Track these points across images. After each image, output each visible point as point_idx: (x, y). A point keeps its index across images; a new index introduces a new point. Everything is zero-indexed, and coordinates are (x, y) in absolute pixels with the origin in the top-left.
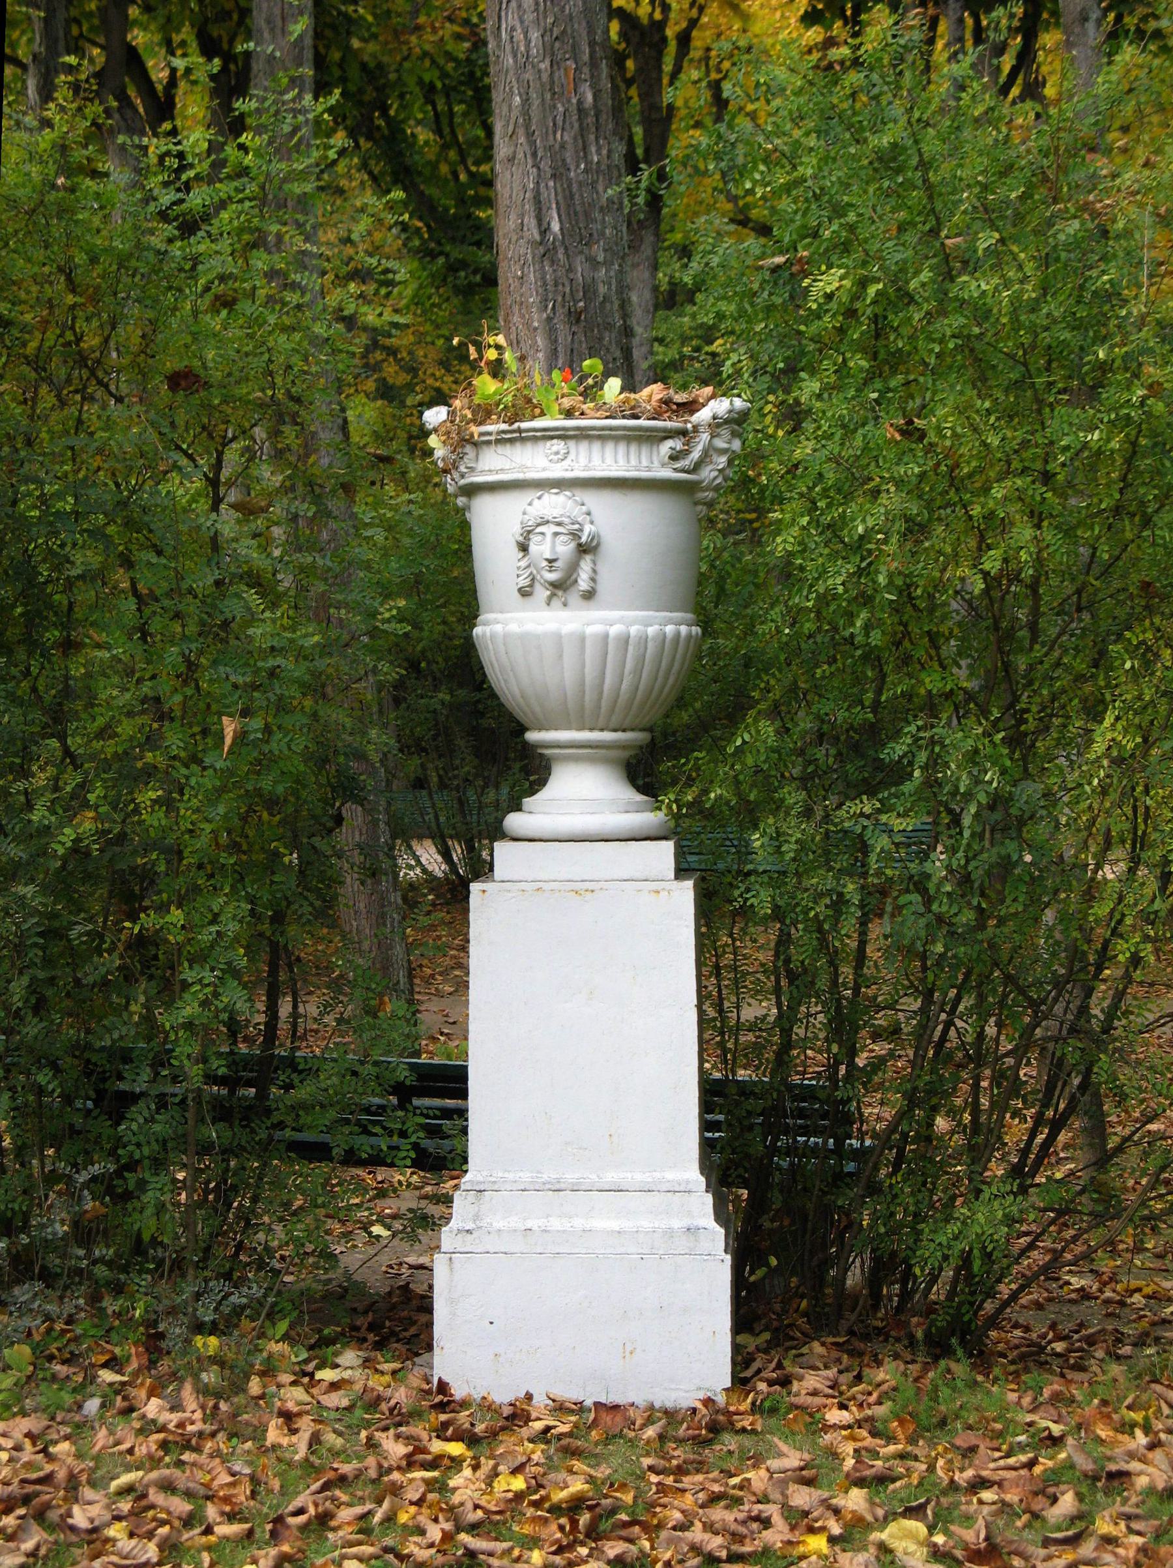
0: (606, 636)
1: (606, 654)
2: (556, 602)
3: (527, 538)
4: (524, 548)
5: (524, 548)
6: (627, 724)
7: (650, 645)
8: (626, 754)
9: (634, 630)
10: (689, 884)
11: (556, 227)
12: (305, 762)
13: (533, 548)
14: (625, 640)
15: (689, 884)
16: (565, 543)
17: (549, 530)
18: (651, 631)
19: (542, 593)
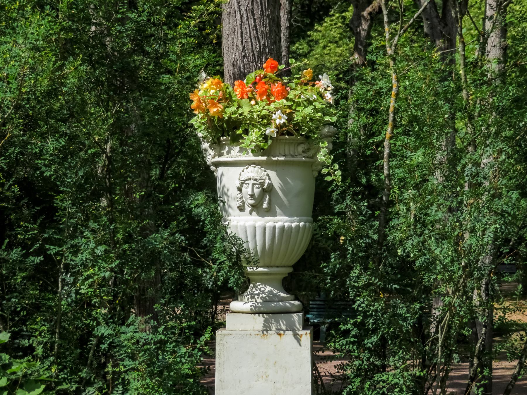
0: (284, 226)
1: (246, 231)
2: (254, 213)
3: (242, 185)
4: (240, 189)
5: (240, 189)
6: (278, 263)
7: (293, 231)
8: (282, 277)
9: (286, 225)
10: (309, 332)
11: (453, 13)
12: (499, 320)
13: (244, 189)
14: (283, 228)
15: (309, 332)
16: (258, 188)
17: (252, 182)
18: (294, 225)
19: (248, 209)
